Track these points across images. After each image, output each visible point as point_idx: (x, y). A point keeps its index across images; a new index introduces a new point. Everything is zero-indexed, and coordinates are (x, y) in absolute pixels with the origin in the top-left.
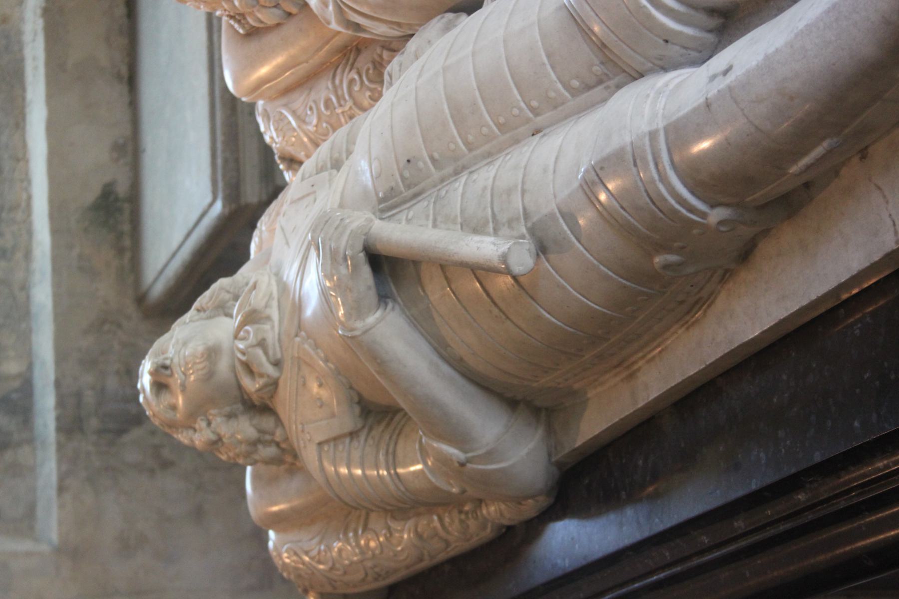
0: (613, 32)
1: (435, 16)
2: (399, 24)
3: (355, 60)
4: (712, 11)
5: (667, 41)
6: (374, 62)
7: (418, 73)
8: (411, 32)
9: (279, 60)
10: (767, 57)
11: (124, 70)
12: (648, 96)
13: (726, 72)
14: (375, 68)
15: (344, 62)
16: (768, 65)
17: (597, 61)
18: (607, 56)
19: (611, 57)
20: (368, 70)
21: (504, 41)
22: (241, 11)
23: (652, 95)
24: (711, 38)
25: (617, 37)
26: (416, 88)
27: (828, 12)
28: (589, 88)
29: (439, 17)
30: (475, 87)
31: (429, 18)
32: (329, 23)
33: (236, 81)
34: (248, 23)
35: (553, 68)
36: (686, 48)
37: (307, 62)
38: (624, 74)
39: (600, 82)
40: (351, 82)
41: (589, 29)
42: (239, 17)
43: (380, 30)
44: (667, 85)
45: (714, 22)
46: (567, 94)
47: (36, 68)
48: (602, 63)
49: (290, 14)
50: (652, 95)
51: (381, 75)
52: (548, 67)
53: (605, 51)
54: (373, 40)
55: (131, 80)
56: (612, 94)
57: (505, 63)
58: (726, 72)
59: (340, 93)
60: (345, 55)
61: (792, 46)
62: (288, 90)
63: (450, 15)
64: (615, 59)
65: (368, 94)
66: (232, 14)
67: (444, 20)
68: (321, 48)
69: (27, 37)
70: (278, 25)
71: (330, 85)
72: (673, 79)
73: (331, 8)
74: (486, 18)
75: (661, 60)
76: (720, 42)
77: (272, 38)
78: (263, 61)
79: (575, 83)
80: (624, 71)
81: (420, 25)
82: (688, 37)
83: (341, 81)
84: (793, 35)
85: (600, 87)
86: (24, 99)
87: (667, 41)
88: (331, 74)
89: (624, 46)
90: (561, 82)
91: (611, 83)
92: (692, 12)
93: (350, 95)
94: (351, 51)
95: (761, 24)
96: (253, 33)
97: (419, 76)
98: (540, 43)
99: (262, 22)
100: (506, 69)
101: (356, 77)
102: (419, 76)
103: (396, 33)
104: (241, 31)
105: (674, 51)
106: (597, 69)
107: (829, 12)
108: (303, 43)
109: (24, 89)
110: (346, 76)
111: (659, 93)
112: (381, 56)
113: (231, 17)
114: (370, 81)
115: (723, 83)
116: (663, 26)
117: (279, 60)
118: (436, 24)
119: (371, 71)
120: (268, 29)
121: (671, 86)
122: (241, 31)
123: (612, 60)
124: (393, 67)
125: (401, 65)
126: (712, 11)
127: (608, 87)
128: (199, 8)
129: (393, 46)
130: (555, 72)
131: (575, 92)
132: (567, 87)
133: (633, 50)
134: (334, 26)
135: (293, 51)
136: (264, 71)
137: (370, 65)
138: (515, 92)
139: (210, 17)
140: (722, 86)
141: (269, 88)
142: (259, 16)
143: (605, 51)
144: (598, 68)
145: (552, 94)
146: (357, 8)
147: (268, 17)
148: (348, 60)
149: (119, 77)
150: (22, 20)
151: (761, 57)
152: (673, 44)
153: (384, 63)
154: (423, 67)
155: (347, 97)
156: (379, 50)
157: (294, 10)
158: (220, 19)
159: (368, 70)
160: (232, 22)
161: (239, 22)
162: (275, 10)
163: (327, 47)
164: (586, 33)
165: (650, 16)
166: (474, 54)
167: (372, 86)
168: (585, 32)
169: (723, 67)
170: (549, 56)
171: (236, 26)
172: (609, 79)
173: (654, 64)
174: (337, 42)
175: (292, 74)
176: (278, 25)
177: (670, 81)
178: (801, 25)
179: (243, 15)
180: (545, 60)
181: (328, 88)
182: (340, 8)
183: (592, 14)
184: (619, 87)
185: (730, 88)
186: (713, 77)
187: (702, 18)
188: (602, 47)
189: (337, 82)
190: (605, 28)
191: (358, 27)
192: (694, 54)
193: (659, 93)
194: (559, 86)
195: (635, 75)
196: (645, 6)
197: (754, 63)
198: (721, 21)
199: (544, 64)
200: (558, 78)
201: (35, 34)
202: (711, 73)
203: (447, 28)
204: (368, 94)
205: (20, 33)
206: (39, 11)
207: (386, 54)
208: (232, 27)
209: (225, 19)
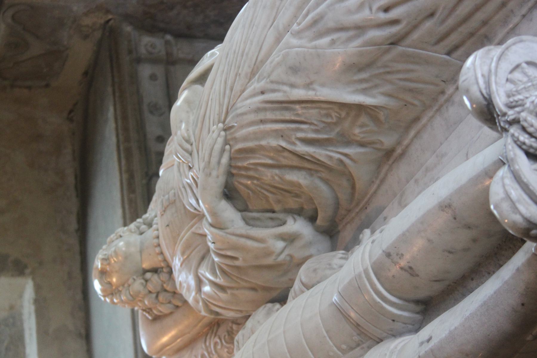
0: (363, 318)
1: (262, 305)
2: (241, 311)
3: (217, 331)
4: (417, 302)
5: (394, 321)
6: (228, 332)
7: (253, 344)
8: (248, 314)
9: (173, 333)
10: (450, 332)
11: (83, 331)
12: (386, 354)
13: (429, 340)
14: (229, 335)
15: (211, 332)
16: (451, 337)
17: (355, 334)
18: (360, 330)
19: (363, 331)
20: (225, 336)
21: (301, 324)
22: (149, 306)
23: (388, 354)
24: (418, 317)
25: (365, 319)
26: (253, 353)
27: (481, 306)
28: (352, 349)
29: (263, 306)
30: (286, 351)
31: (258, 307)
32: (200, 312)
33: (148, 347)
34: (153, 313)
35: (330, 338)
36: (405, 324)
37: (189, 333)
38: (371, 341)
39: (358, 345)
40: (216, 344)
41: (349, 316)
42: (149, 310)
43: (230, 314)
44: (396, 348)
45: (419, 308)
46: (340, 353)
47: (31, 335)
48: (358, 335)
49: (177, 307)
50: (388, 354)
51: (232, 339)
52: (328, 338)
53: (359, 328)
54: (226, 320)
55: (87, 336)
56: (366, 352)
57: (302, 337)
58: (429, 340)
59: (209, 350)
60: (211, 328)
61: (464, 326)
62: (179, 350)
63: (270, 305)
64: (365, 332)
65: (226, 350)
66: (144, 308)
67: (266, 308)
68: (196, 326)
69: (25, 316)
70: (171, 313)
71: (203, 346)
72: (400, 343)
73: (201, 304)
74: (290, 311)
75: (392, 331)
76: (424, 318)
77: (168, 321)
78: (164, 334)
79: (344, 347)
80: (371, 339)
81: (254, 311)
82: (405, 317)
83: (210, 344)
84: (463, 319)
85: (359, 348)
86: (24, 353)
87: (394, 321)
88: (204, 340)
89: (369, 325)
90: (336, 347)
91: (364, 345)
92: (406, 304)
93: (216, 352)
94: (214, 325)
95: (445, 311)
96: (157, 318)
97: (254, 346)
98: (321, 325)
99: (161, 312)
100: (304, 340)
101: (218, 341)
102: (254, 346)
103: (239, 315)
104: (150, 318)
105: (398, 326)
106: (356, 338)
107: (482, 306)
108: (186, 323)
109: (24, 347)
110: (212, 341)
111: (392, 352)
112: (232, 328)
113: (144, 310)
114: (226, 342)
115: (427, 347)
116: (390, 312)
117: (173, 333)
118: (261, 312)
119: (227, 337)
120: (166, 316)
121: (399, 348)
122: (150, 318)
123: (363, 333)
124: (239, 337)
125: (243, 336)
126: (417, 302)
127: (363, 348)
128: (125, 306)
129: (240, 322)
130: (331, 341)
131: (344, 352)
132: (339, 348)
133: (375, 327)
134: (203, 313)
135: (181, 327)
136: (165, 339)
137: (226, 333)
138: (310, 353)
139: (133, 311)
140: (427, 349)
141: (169, 349)
142: (160, 309)
143: (359, 328)
144: (356, 337)
145: (331, 354)
146: (216, 303)
147: (164, 309)
148: (213, 331)
149: (80, 335)
150: (22, 306)
151: (447, 332)
152: (397, 322)
153: (234, 332)
154: (256, 340)
155: (214, 352)
156: (230, 324)
157: (179, 304)
158: (138, 311)
159: (225, 336)
160: (145, 313)
161: (148, 313)
162: (169, 305)
163: (200, 324)
164: (348, 319)
165: (383, 308)
166: (284, 332)
167: (228, 345)
168: (346, 317)
169: (427, 338)
170: (327, 332)
171: (147, 315)
172: (363, 343)
173: (388, 334)
174: (205, 321)
175: (181, 341)
176: (171, 313)
177: (397, 345)
178: (467, 314)
179: (150, 309)
180: (326, 335)
181: (202, 348)
182: (206, 304)
183: (350, 308)
184: (369, 348)
185: (432, 350)
186: (422, 343)
187: (412, 306)
188: (357, 326)
189: (208, 344)
190: (358, 315)
191: (217, 314)
192: (410, 327)
193: (392, 352)
194: (335, 349)
195: (378, 340)
196: (379, 302)
197: (444, 335)
198: (424, 307)
199: (325, 337)
200: (334, 344)
201: (30, 314)
202: (420, 340)
203: (269, 314)
204: (226, 350)
205: (21, 314)
206: (32, 301)
207: (235, 327)
208: (145, 316)
209: (140, 311)
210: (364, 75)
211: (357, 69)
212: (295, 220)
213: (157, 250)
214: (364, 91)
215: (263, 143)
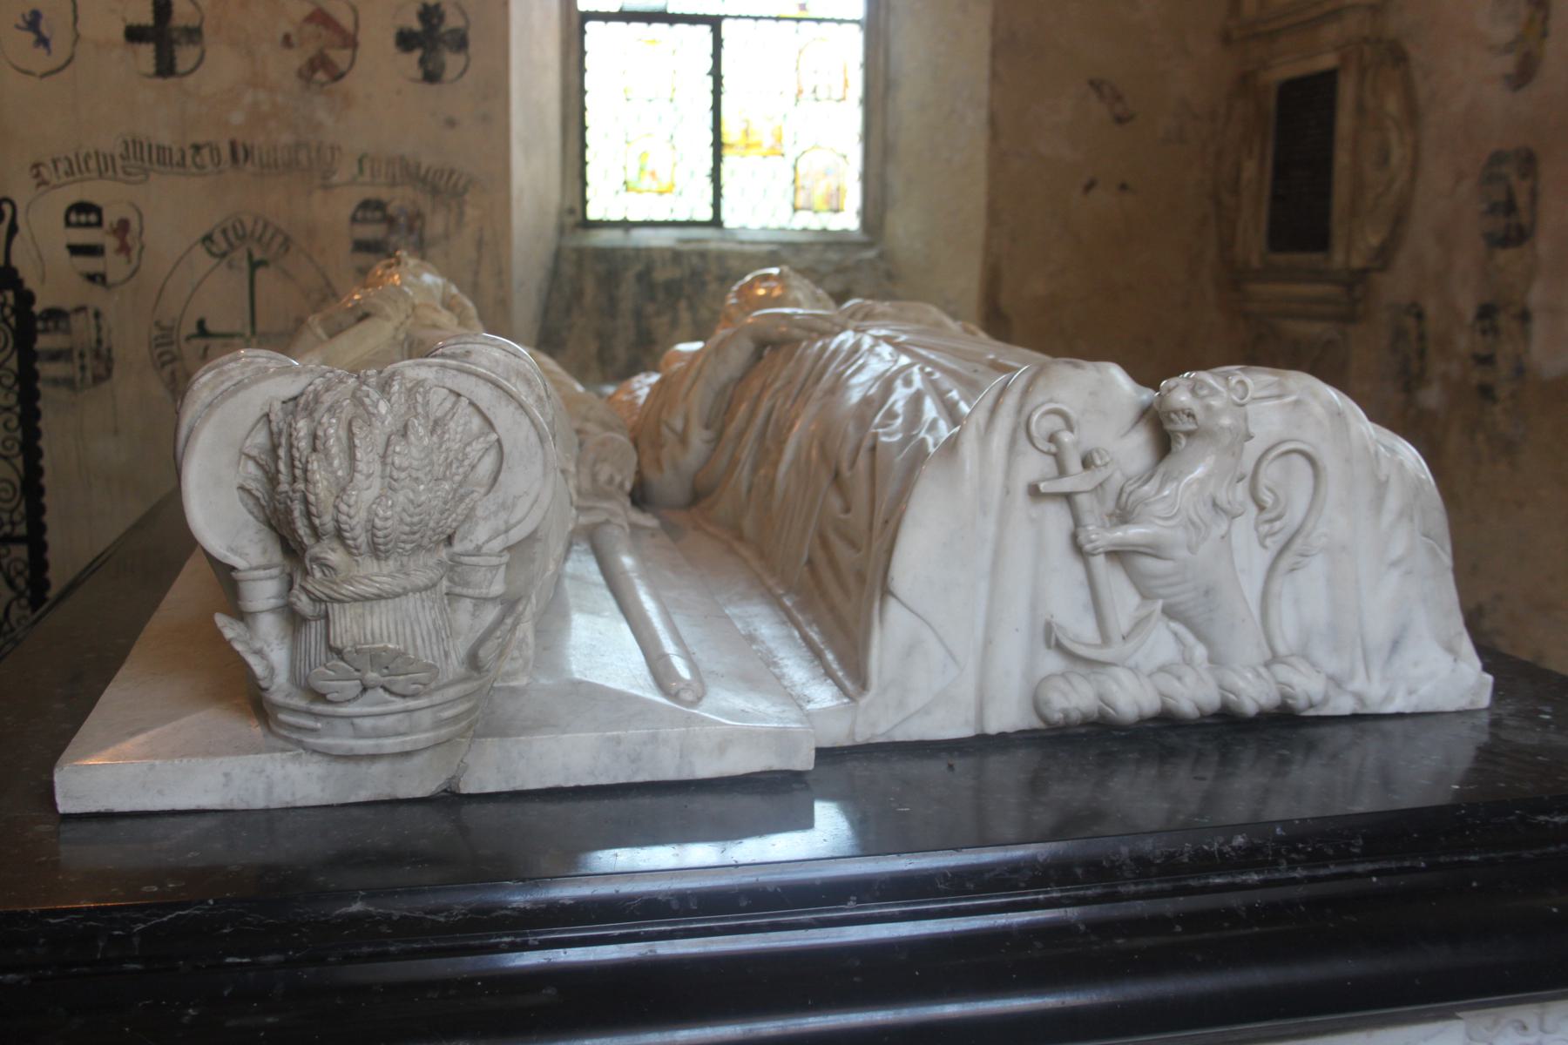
210: (814, 453)
211: (825, 440)
212: (708, 442)
213: (1476, 376)
214: (796, 461)
215: (792, 364)
